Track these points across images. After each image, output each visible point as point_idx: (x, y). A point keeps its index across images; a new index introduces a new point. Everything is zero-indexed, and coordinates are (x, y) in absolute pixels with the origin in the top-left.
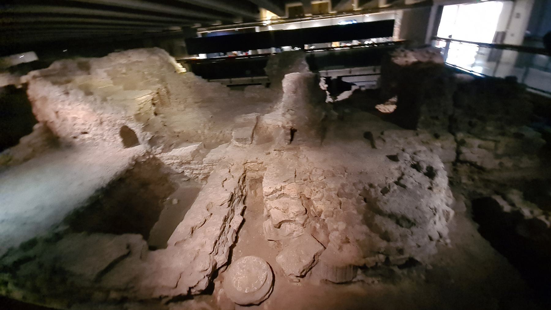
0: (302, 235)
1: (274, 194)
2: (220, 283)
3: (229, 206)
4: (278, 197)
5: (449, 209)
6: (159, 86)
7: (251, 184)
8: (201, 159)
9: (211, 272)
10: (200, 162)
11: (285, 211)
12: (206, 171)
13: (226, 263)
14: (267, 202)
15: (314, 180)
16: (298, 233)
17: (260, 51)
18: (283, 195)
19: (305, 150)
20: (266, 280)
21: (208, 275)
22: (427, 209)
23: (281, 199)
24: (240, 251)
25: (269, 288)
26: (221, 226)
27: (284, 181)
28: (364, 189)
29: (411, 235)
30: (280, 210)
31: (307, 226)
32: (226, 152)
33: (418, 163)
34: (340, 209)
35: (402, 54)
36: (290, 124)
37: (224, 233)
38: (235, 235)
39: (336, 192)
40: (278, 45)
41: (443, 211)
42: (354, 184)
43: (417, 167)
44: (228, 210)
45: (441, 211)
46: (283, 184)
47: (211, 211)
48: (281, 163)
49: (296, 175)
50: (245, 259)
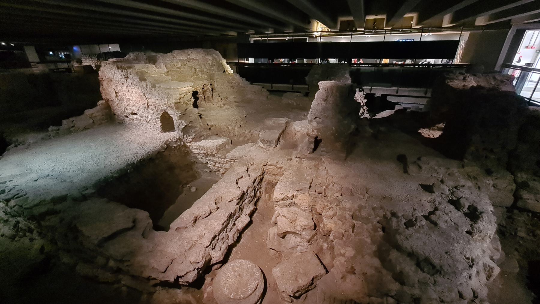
0: (307, 251)
1: (284, 202)
2: (211, 280)
3: (238, 204)
4: (288, 206)
5: (492, 264)
6: (205, 82)
7: (267, 187)
8: (225, 153)
9: (202, 266)
10: (223, 156)
11: (293, 221)
12: (227, 166)
13: (221, 261)
14: (276, 208)
15: (329, 195)
16: (302, 248)
17: (305, 61)
18: (294, 204)
19: (326, 162)
20: (255, 290)
21: (200, 269)
22: (459, 257)
23: (291, 208)
24: (239, 253)
25: (257, 299)
26: (223, 222)
27: (297, 189)
28: (385, 216)
29: (434, 285)
30: (287, 219)
31: (313, 243)
32: (250, 151)
33: (459, 199)
34: (352, 233)
35: (461, 77)
36: (315, 133)
37: (226, 229)
38: (237, 235)
39: (351, 213)
40: (324, 57)
41: (485, 265)
42: (374, 209)
43: (456, 204)
44: (235, 208)
45: (480, 263)
46: (295, 193)
47: (218, 205)
48: (299, 172)
49: (310, 187)
50: (240, 261)
